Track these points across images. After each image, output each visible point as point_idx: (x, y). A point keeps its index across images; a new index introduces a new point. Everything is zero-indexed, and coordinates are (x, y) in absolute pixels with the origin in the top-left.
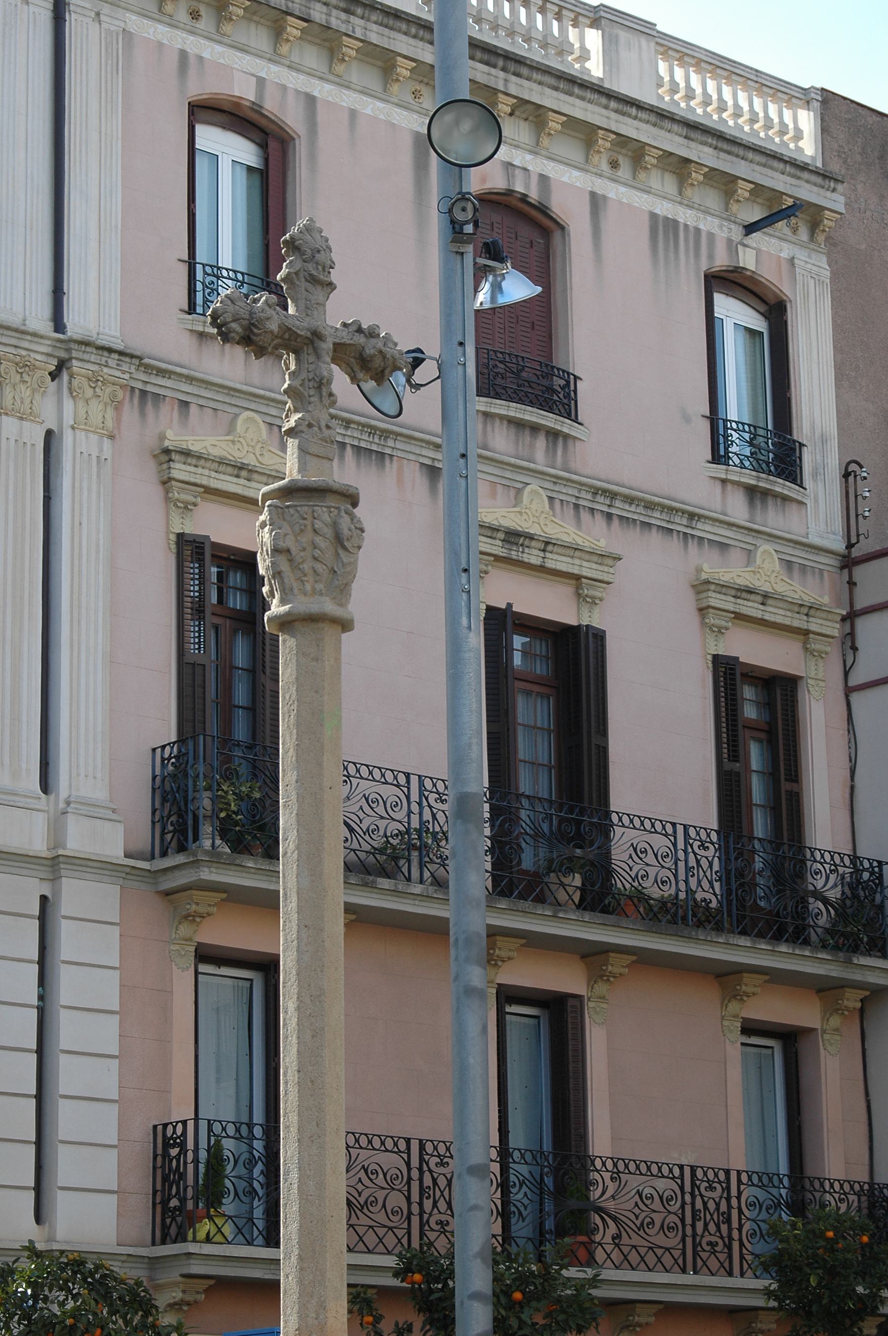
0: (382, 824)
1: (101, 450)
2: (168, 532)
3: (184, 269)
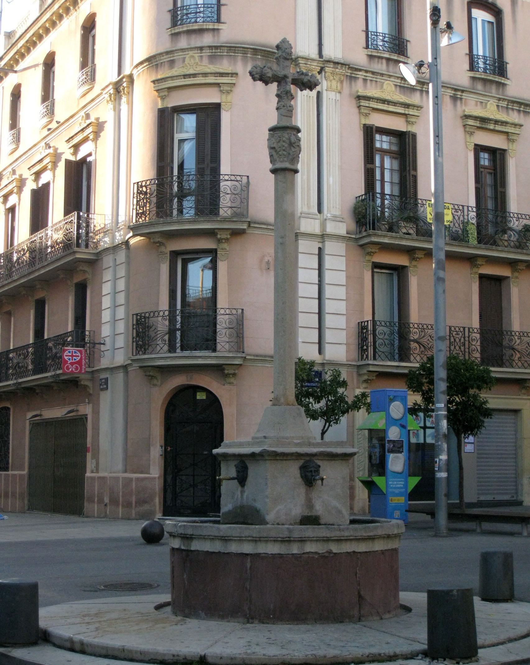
1: (336, 97)
2: (360, 124)
3: (364, 34)
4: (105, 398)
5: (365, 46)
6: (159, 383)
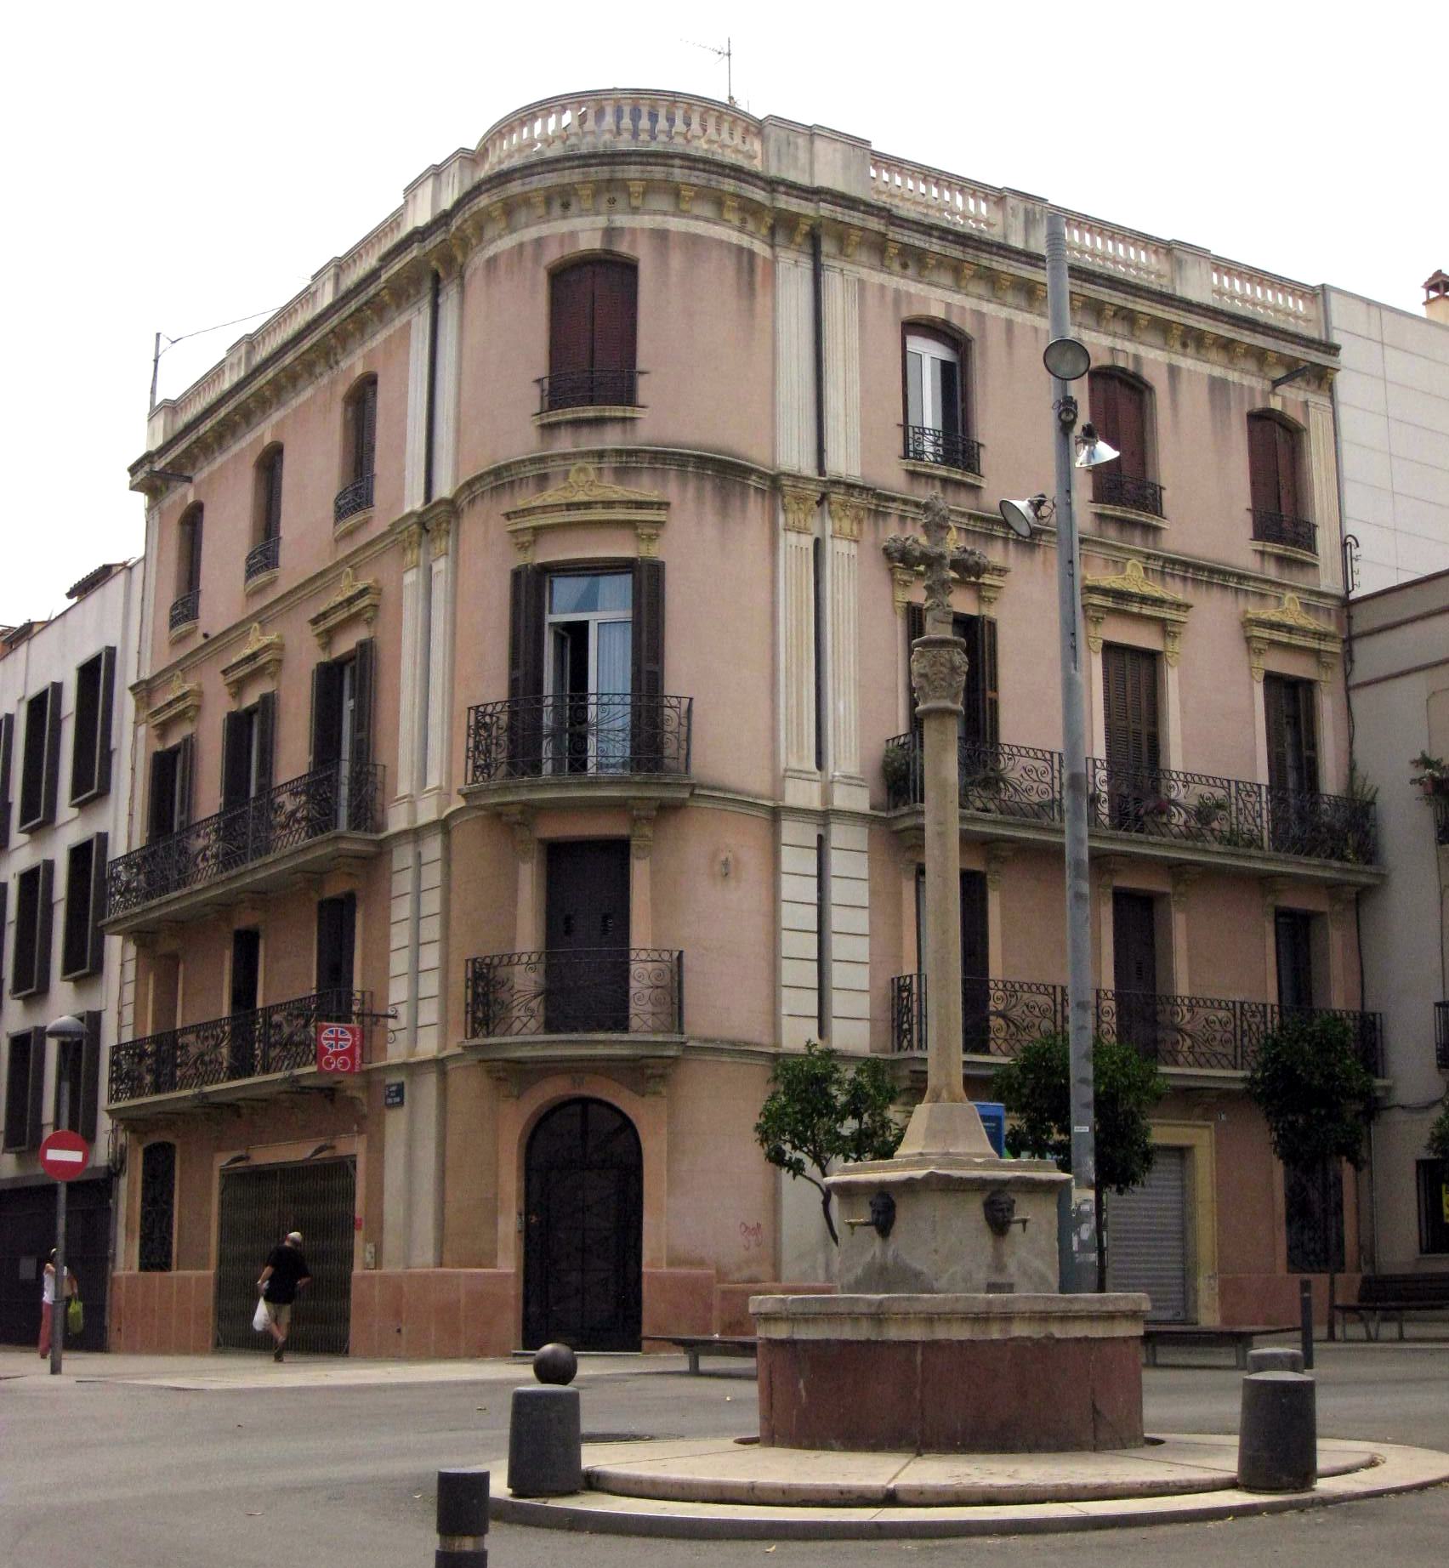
0: (1035, 785)
4: (396, 1123)
5: (902, 453)
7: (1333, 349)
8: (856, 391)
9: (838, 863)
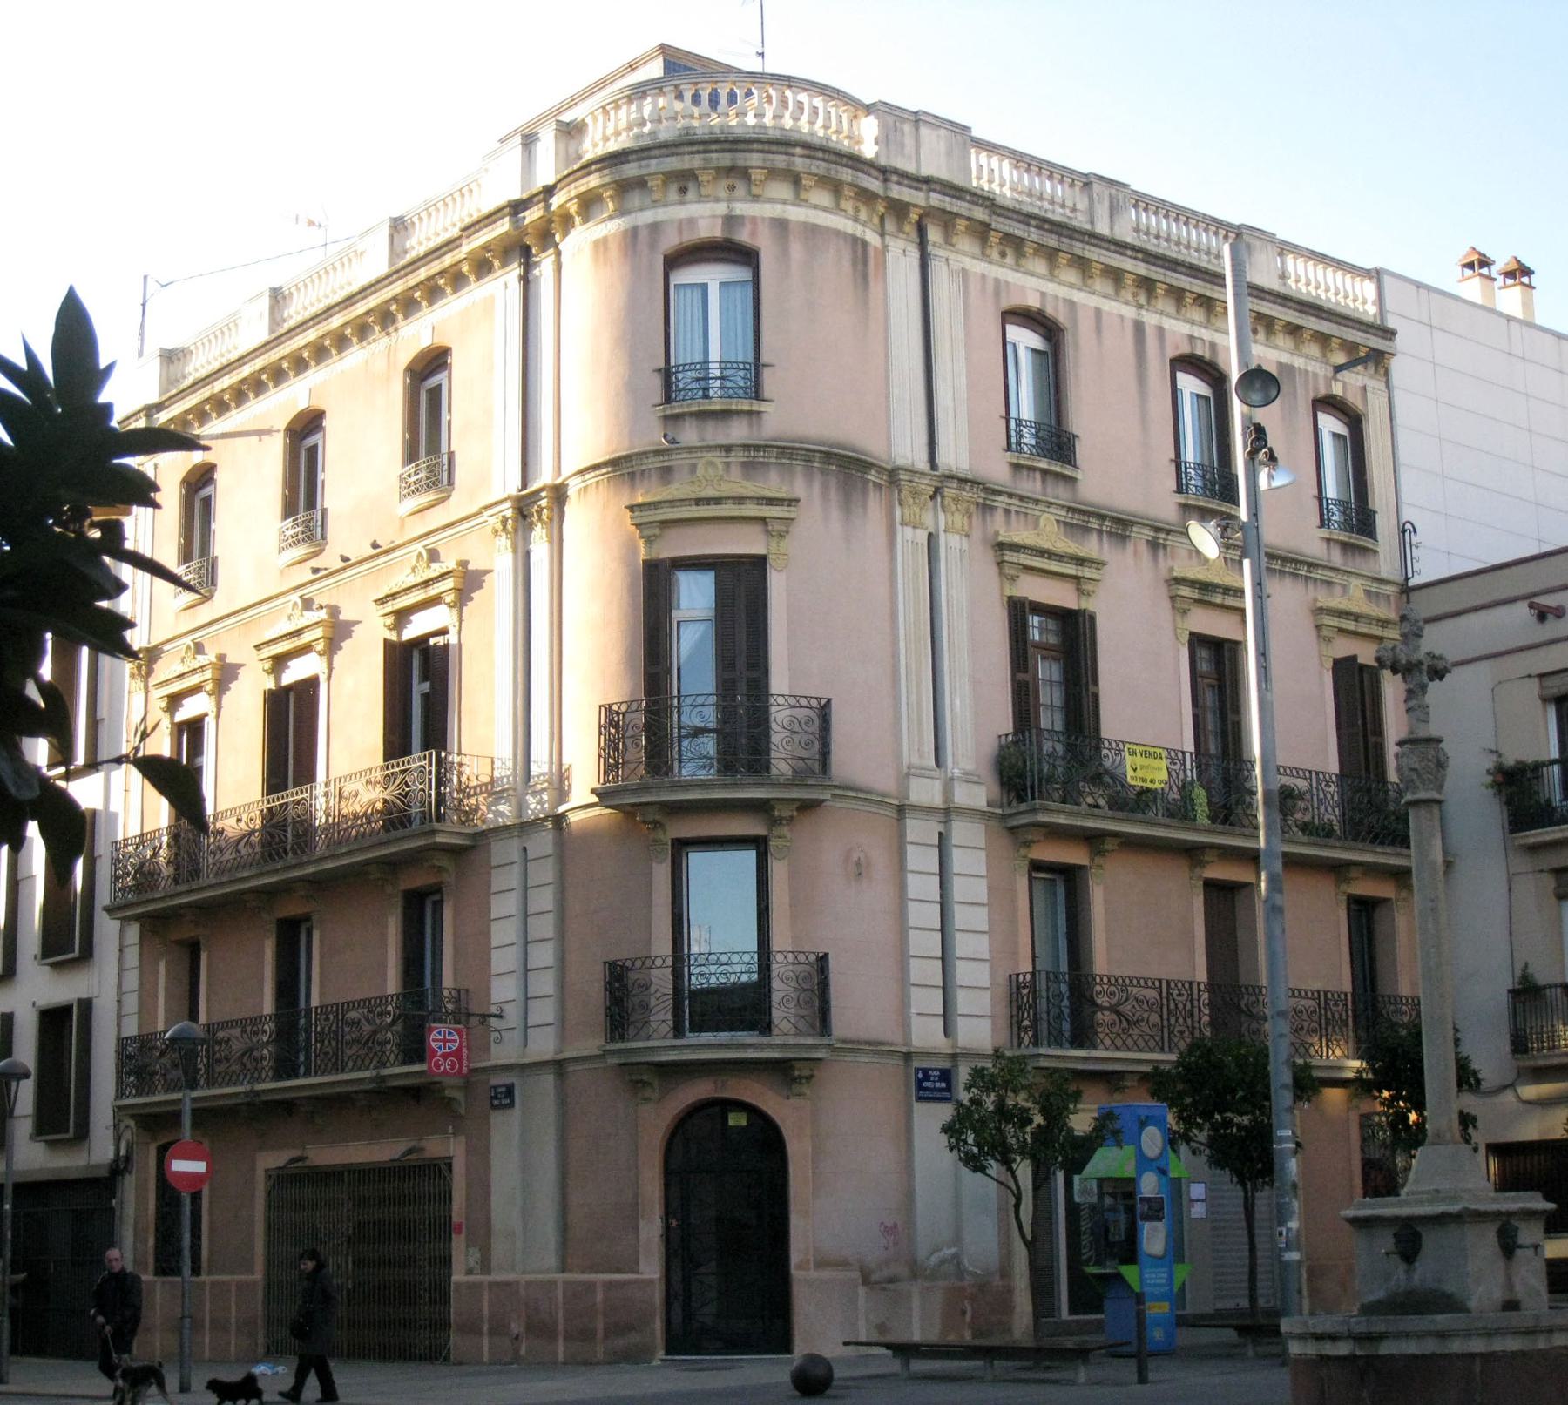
6: (655, 1096)
7: (1389, 334)
8: (963, 381)
9: (960, 860)
